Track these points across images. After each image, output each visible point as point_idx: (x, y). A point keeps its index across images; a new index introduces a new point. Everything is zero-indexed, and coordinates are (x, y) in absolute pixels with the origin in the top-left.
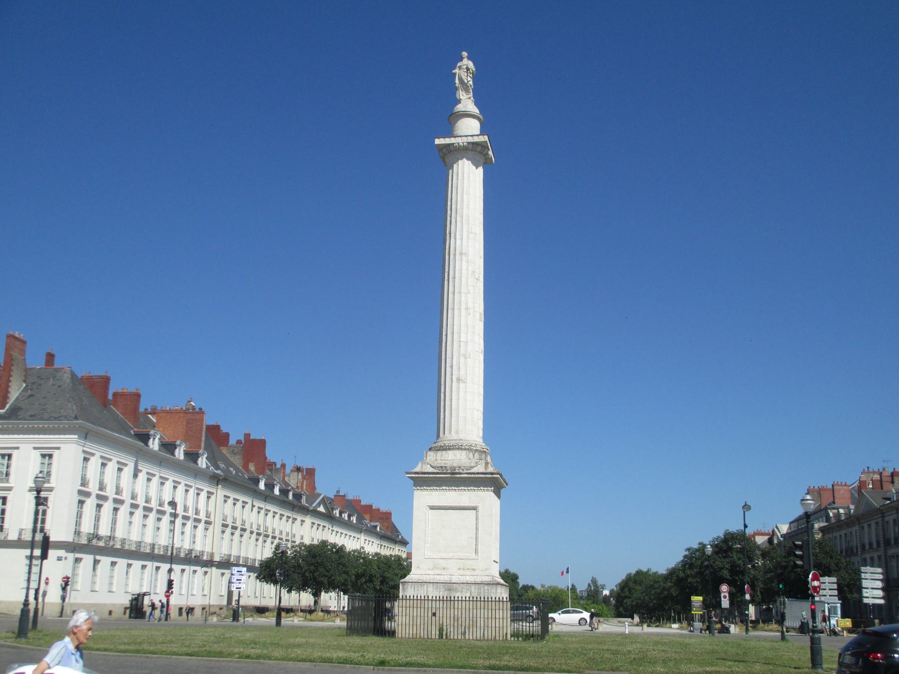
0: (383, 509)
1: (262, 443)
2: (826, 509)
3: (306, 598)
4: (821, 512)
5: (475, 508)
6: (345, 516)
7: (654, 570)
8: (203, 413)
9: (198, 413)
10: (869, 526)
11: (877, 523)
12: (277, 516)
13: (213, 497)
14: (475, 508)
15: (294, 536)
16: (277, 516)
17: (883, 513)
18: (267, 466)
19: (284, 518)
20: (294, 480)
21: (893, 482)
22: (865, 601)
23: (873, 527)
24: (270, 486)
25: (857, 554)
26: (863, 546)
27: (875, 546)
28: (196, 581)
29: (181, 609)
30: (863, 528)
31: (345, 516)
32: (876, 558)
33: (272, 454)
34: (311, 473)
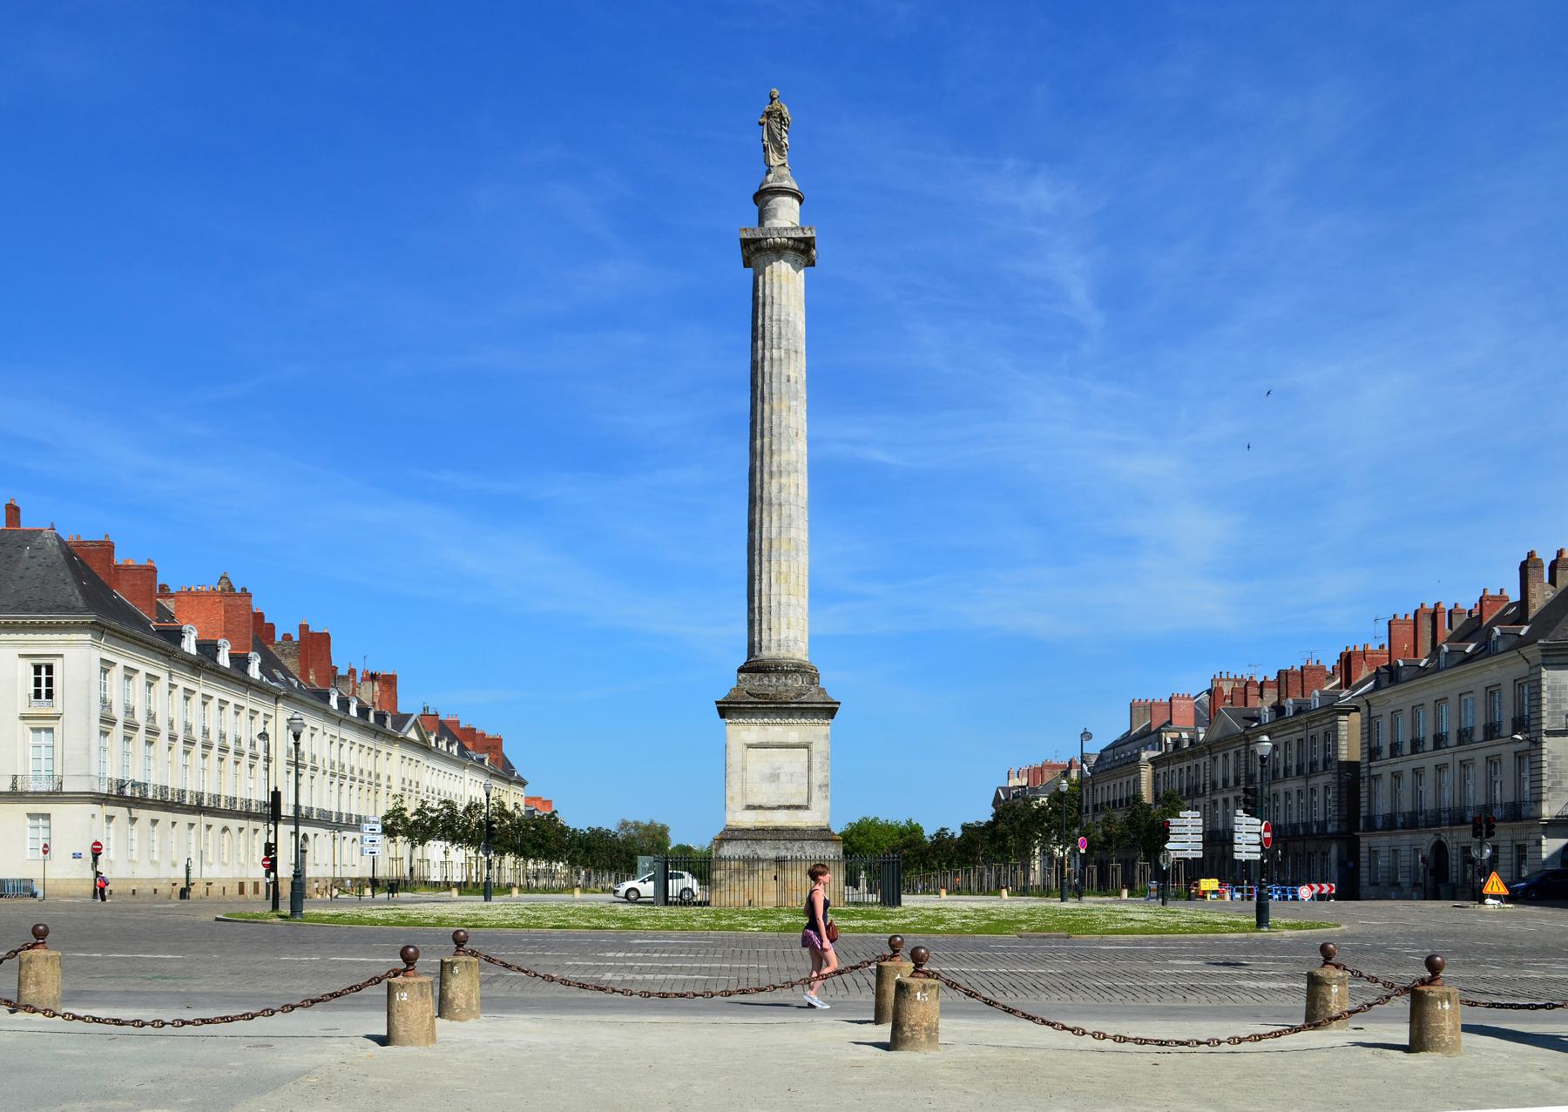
0: (490, 734)
1: (325, 638)
2: (1159, 731)
3: (543, 865)
4: (1149, 736)
5: (807, 746)
6: (443, 744)
7: (882, 819)
8: (250, 595)
9: (239, 595)
10: (1226, 756)
11: (1238, 753)
12: (356, 748)
13: (271, 722)
14: (807, 746)
15: (378, 776)
16: (356, 748)
17: (1248, 739)
18: (331, 676)
19: (365, 750)
20: (369, 693)
21: (1261, 696)
22: (1237, 856)
23: (1232, 757)
24: (344, 704)
25: (1204, 794)
26: (1214, 785)
27: (1231, 783)
28: (210, 842)
29: (242, 886)
30: (1215, 759)
31: (443, 744)
32: (1232, 801)
33: (341, 660)
34: (389, 682)
